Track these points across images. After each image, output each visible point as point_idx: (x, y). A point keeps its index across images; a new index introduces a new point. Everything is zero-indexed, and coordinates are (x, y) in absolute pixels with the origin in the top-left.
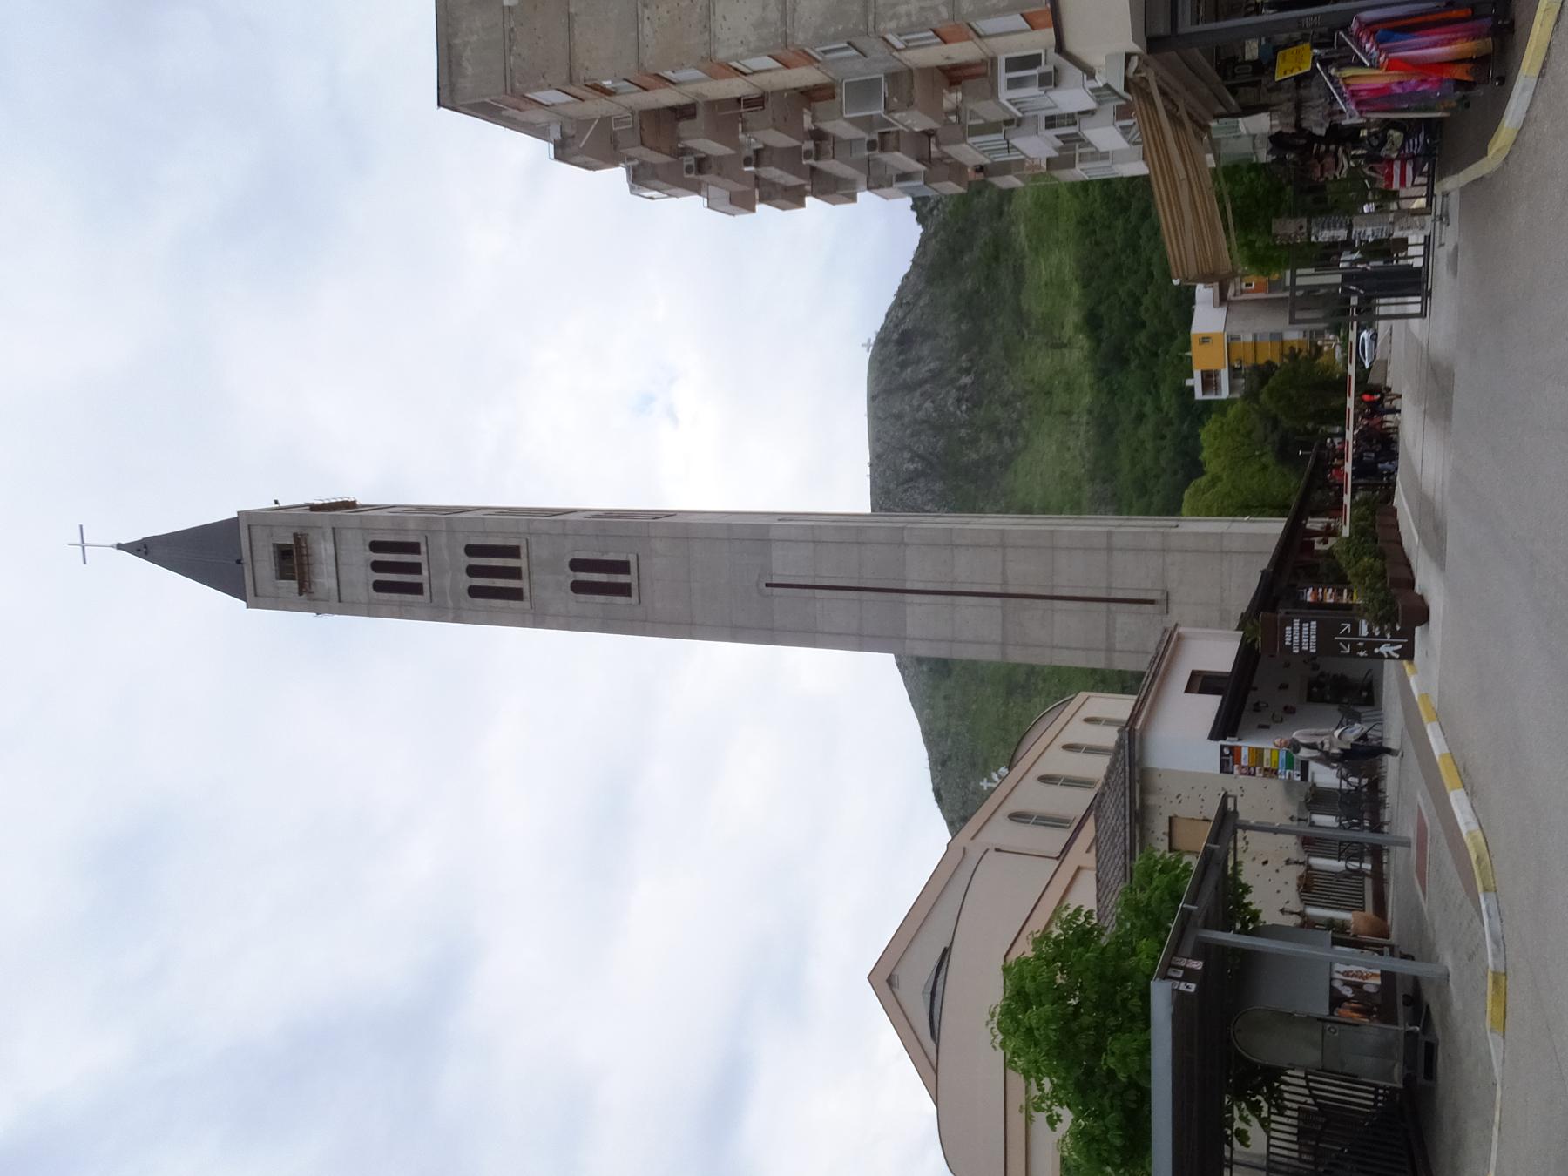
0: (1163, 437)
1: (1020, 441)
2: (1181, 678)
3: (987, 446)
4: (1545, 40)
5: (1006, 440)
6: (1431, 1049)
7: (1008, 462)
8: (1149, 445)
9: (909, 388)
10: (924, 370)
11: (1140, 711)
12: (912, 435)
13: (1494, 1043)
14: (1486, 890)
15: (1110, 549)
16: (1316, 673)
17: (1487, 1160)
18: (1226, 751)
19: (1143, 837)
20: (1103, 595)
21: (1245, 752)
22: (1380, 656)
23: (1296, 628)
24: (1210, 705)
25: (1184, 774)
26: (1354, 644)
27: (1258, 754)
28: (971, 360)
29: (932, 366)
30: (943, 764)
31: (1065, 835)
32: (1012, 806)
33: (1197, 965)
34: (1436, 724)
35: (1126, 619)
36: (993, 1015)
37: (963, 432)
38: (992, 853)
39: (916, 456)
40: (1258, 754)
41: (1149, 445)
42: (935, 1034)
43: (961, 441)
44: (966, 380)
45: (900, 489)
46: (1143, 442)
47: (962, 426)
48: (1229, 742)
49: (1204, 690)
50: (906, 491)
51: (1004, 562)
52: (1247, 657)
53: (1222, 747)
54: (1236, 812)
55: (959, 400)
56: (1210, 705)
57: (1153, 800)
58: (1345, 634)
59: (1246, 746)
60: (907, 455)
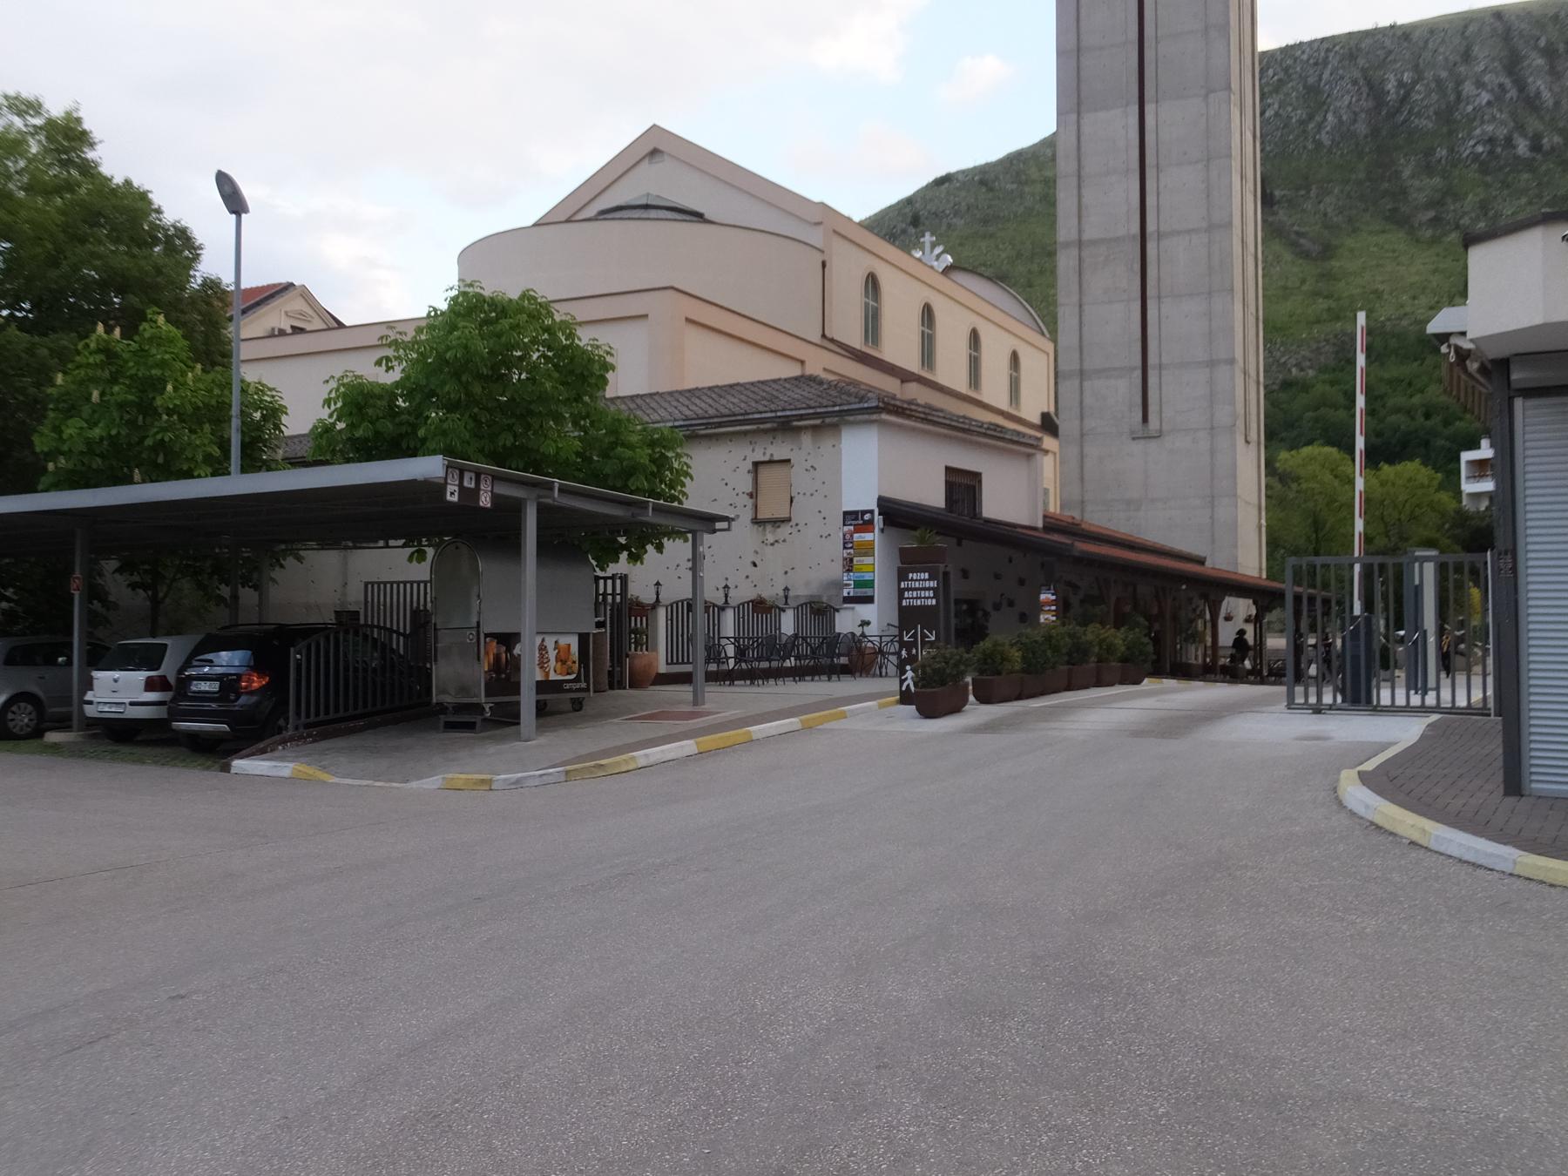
0: (1427, 416)
1: (1428, 233)
2: (966, 460)
3: (1422, 188)
4: (1399, 830)
5: (1431, 214)
6: (470, 726)
7: (1398, 219)
8: (1416, 399)
9: (1513, 65)
10: (1539, 84)
11: (909, 417)
12: (1439, 81)
13: (431, 783)
14: (567, 772)
15: (1212, 364)
16: (989, 608)
17: (348, 776)
18: (867, 517)
19: (766, 431)
20: (1152, 359)
21: (868, 537)
22: (903, 672)
23: (927, 584)
24: (933, 495)
25: (838, 472)
26: (914, 644)
27: (867, 550)
28: (1553, 149)
29: (1546, 95)
30: (982, 183)
31: (856, 340)
32: (887, 277)
33: (485, 501)
34: (799, 726)
35: (1124, 389)
36: (471, 285)
37: (1442, 152)
38: (819, 258)
39: (1406, 90)
40: (867, 550)
41: (1416, 399)
42: (605, 214)
43: (1430, 152)
44: (1522, 146)
45: (1357, 74)
46: (1422, 392)
47: (1451, 150)
48: (878, 520)
49: (950, 487)
50: (1355, 82)
51: (1189, 232)
52: (1003, 536)
53: (871, 512)
54: (714, 531)
55: (1491, 140)
56: (933, 495)
57: (806, 439)
58: (924, 636)
59: (874, 537)
60: (1407, 77)
